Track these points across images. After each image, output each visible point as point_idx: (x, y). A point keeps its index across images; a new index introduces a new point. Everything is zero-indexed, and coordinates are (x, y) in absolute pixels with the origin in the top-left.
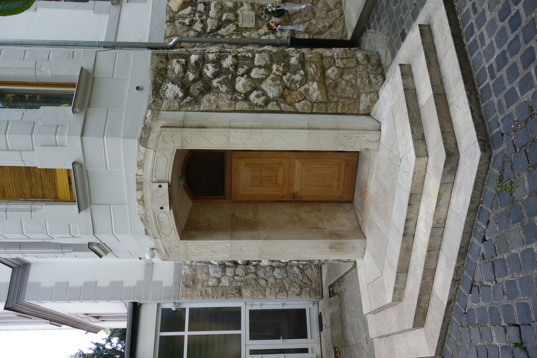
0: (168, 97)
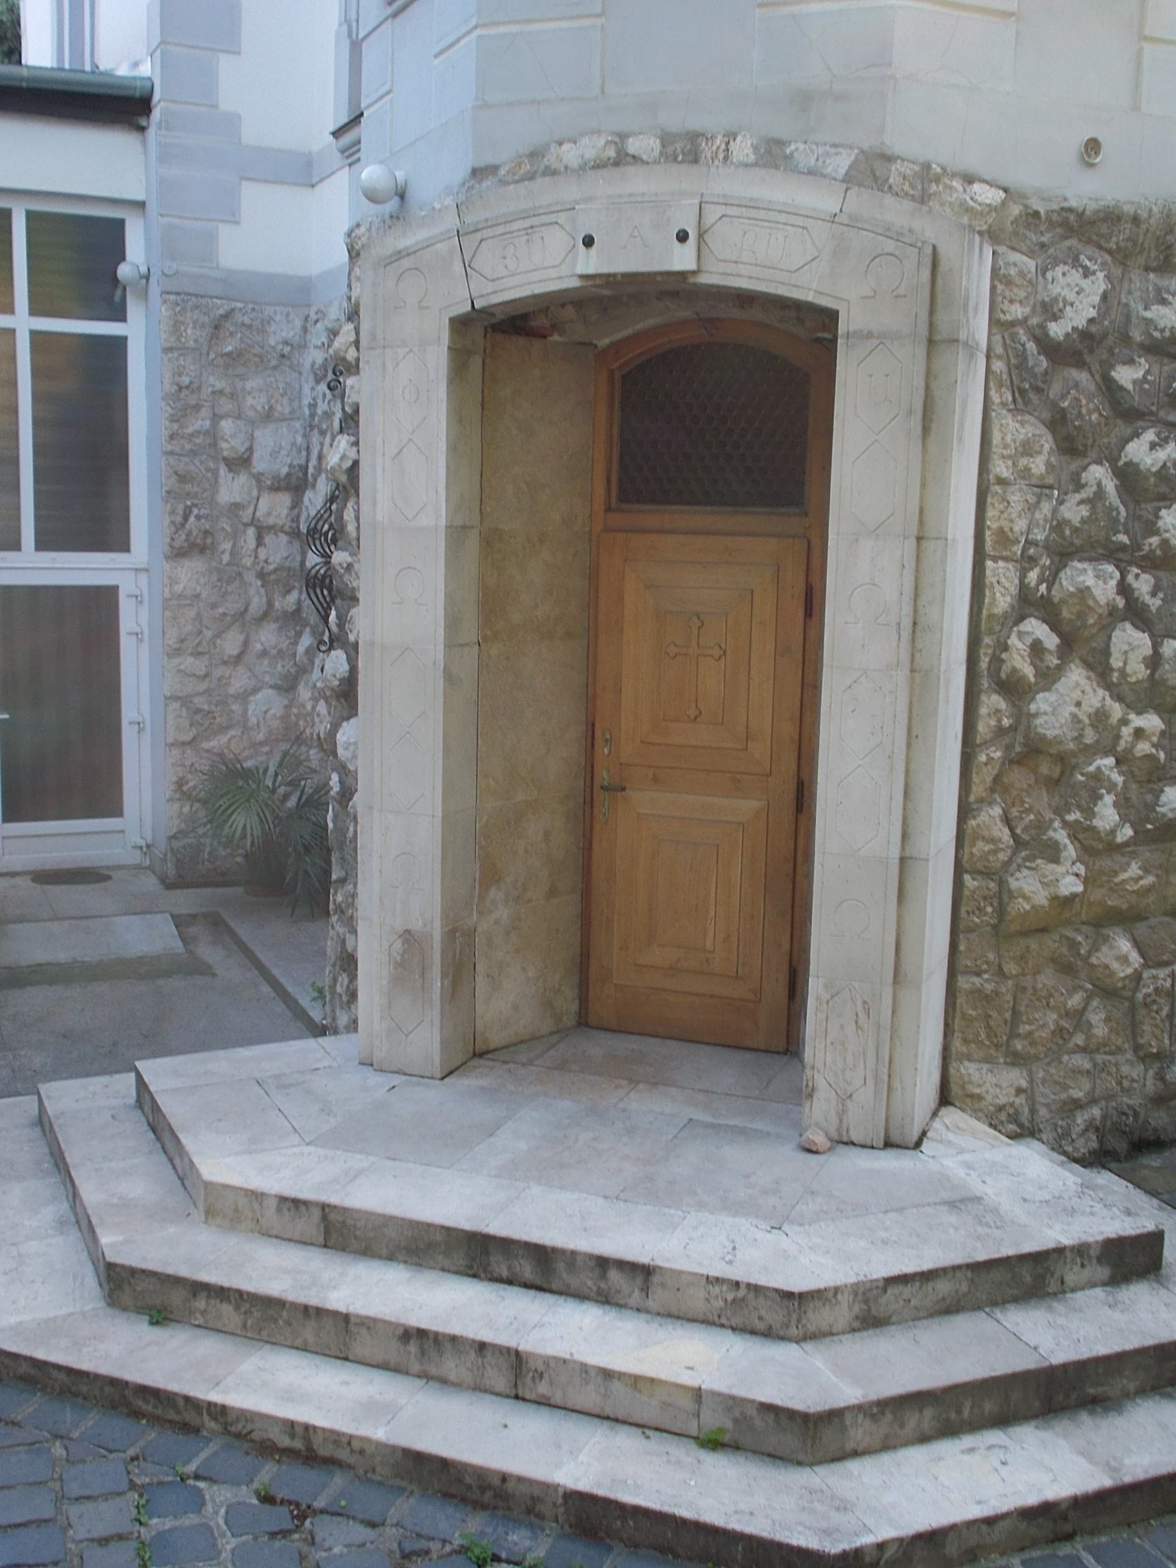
0: (1049, 275)
